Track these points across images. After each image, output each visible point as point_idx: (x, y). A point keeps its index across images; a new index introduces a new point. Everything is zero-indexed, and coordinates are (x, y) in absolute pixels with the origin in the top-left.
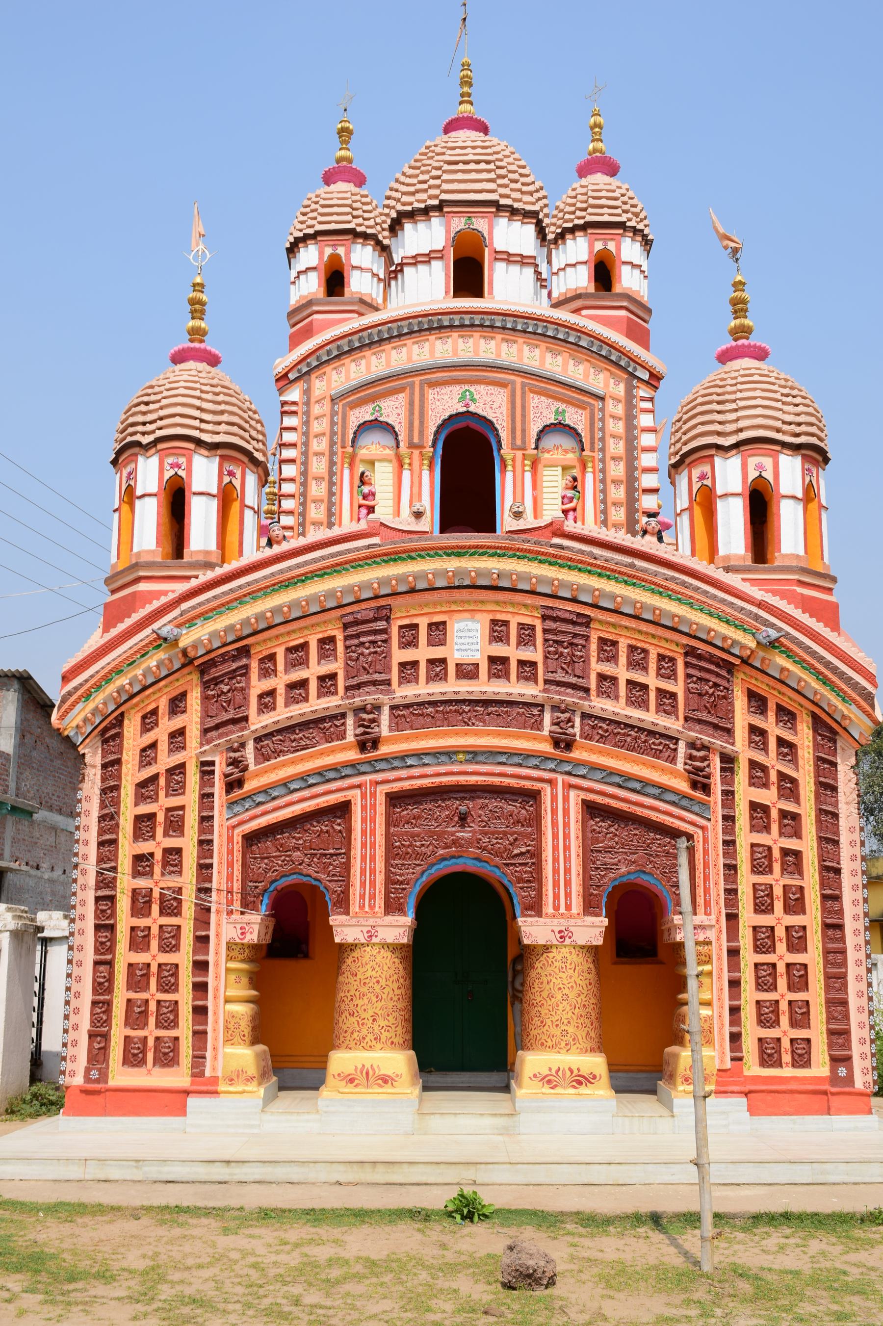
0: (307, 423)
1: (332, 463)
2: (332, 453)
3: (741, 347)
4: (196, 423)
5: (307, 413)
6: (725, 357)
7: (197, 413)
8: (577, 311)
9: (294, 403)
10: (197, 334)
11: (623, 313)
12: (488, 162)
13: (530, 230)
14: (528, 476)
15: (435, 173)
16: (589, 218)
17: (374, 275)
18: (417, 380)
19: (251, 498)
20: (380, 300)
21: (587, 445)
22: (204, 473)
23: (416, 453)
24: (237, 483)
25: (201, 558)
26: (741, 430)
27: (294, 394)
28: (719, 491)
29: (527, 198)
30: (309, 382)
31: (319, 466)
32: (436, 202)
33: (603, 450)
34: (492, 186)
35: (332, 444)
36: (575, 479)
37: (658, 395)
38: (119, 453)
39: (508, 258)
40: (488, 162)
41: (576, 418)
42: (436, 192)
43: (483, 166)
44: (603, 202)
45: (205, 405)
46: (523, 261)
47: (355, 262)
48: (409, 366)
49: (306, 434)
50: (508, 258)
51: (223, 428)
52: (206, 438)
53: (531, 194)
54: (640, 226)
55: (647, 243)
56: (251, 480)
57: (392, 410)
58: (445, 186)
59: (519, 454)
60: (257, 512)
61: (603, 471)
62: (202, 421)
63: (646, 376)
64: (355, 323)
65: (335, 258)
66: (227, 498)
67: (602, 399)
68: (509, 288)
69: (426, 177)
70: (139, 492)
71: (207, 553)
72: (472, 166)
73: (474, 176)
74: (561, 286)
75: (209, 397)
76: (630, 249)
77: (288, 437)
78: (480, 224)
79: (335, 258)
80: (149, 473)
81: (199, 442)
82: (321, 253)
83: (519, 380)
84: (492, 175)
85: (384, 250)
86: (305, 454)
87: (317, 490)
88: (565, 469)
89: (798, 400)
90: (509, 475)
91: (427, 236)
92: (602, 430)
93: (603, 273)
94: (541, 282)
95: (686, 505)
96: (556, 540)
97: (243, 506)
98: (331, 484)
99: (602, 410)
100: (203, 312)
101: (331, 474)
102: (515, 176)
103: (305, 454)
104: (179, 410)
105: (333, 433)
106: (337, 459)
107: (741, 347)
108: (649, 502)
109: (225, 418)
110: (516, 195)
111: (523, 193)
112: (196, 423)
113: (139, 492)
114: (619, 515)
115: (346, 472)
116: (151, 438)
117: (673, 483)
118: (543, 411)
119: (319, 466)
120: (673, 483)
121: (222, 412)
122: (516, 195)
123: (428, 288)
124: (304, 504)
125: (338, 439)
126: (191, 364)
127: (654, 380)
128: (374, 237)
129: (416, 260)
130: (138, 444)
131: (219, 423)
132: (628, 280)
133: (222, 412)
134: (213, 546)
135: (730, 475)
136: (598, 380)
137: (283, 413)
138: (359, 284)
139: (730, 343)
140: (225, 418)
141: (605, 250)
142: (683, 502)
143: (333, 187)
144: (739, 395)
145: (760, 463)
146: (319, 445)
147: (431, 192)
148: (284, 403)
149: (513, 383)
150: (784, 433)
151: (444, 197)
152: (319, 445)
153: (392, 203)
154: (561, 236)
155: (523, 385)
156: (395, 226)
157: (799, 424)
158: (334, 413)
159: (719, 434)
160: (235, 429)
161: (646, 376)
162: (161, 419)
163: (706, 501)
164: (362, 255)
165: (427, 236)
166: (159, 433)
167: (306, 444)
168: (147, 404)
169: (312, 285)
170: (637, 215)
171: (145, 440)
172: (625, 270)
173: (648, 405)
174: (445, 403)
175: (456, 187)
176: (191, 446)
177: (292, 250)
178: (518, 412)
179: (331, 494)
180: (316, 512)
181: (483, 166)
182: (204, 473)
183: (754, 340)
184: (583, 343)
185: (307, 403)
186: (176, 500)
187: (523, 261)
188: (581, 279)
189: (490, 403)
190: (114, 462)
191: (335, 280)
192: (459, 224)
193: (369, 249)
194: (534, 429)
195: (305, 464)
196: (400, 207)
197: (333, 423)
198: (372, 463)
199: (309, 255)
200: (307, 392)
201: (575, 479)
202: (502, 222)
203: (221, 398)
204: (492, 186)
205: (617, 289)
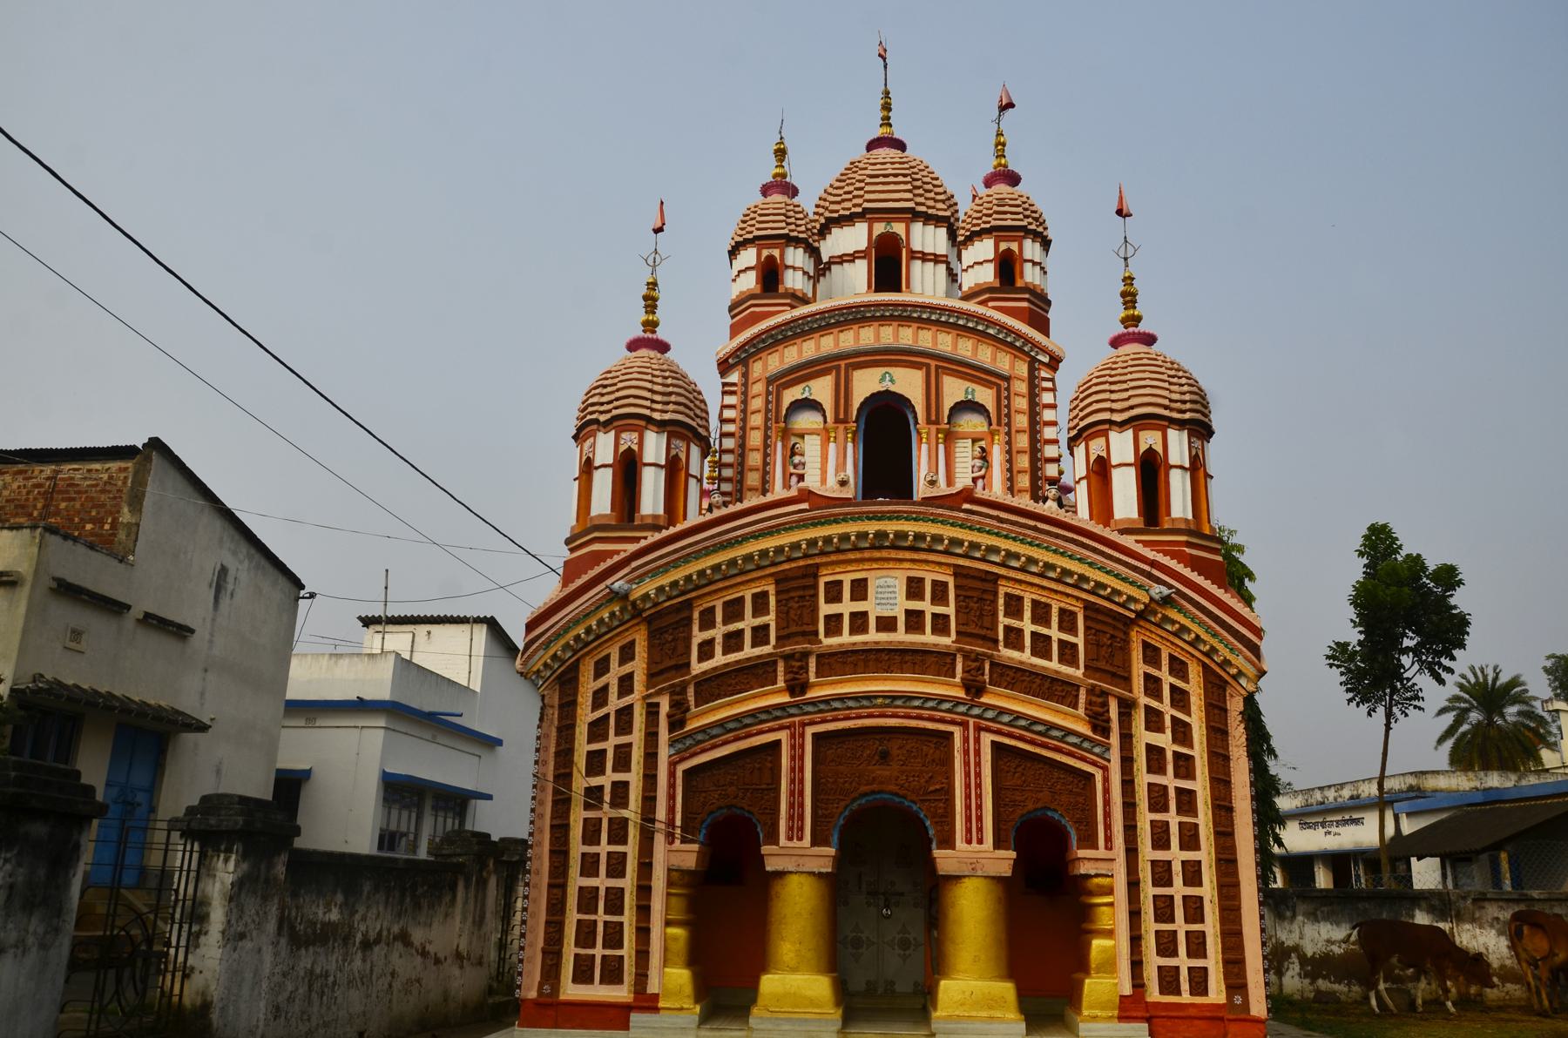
0: (745, 402)
1: (766, 437)
2: (767, 428)
3: (1133, 334)
4: (648, 403)
5: (745, 393)
6: (1116, 342)
7: (648, 395)
8: (980, 303)
9: (734, 384)
10: (651, 325)
11: (1025, 304)
12: (905, 175)
13: (942, 232)
14: (941, 447)
15: (858, 185)
16: (994, 223)
17: (805, 273)
18: (843, 363)
19: (694, 470)
20: (810, 295)
21: (994, 420)
22: (654, 447)
23: (841, 427)
24: (683, 456)
25: (649, 521)
26: (1132, 407)
27: (734, 377)
28: (1114, 462)
29: (940, 205)
30: (747, 366)
31: (755, 438)
32: (859, 210)
33: (1009, 425)
34: (909, 195)
35: (767, 419)
36: (983, 449)
37: (1058, 376)
38: (580, 429)
39: (924, 257)
40: (905, 175)
41: (985, 396)
42: (859, 201)
43: (901, 179)
44: (1006, 209)
45: (657, 388)
46: (937, 259)
47: (789, 262)
48: (836, 351)
49: (744, 411)
50: (924, 257)
51: (671, 407)
52: (657, 416)
53: (943, 201)
54: (1040, 229)
55: (1046, 244)
56: (695, 451)
57: (821, 388)
58: (867, 196)
59: (933, 428)
60: (700, 481)
61: (1009, 443)
62: (653, 401)
63: (1046, 359)
64: (788, 315)
65: (771, 258)
66: (674, 469)
67: (1007, 379)
68: (926, 285)
69: (851, 188)
70: (597, 464)
71: (655, 517)
72: (891, 179)
73: (892, 187)
74: (968, 281)
75: (659, 380)
76: (1031, 249)
77: (728, 414)
78: (899, 228)
79: (771, 258)
80: (605, 447)
81: (649, 420)
82: (759, 255)
83: (933, 363)
84: (909, 187)
85: (814, 252)
86: (743, 428)
87: (755, 459)
88: (974, 441)
89: (1183, 381)
90: (924, 447)
91: (853, 238)
92: (1008, 406)
93: (1007, 266)
94: (952, 276)
95: (1084, 473)
96: (966, 506)
97: (688, 475)
98: (766, 455)
99: (1008, 389)
100: (655, 307)
101: (766, 446)
102: (929, 187)
103: (743, 428)
104: (631, 401)
105: (767, 411)
106: (772, 433)
107: (1133, 334)
108: (1051, 470)
109: (673, 398)
110: (931, 203)
111: (936, 201)
112: (648, 403)
113: (597, 464)
114: (1024, 481)
115: (779, 445)
116: (608, 416)
117: (1072, 454)
118: (954, 390)
119: (755, 438)
120: (1072, 454)
121: (670, 394)
122: (931, 203)
123: (854, 283)
124: (741, 473)
125: (772, 415)
126: (643, 352)
127: (1055, 362)
128: (804, 241)
129: (842, 260)
130: (596, 421)
131: (667, 403)
132: (1030, 275)
133: (670, 394)
134: (661, 511)
135: (1122, 447)
136: (1003, 362)
137: (724, 393)
138: (794, 281)
139: (1120, 329)
140: (673, 398)
141: (1009, 250)
142: (1081, 471)
143: (769, 199)
144: (1129, 377)
145: (1151, 439)
146: (756, 420)
147: (856, 201)
148: (724, 385)
149: (928, 366)
150: (1172, 410)
151: (866, 205)
152: (756, 420)
153: (821, 210)
154: (970, 239)
155: (937, 367)
156: (824, 231)
157: (1184, 402)
158: (768, 393)
159: (1112, 411)
160: (681, 408)
161: (1046, 359)
162: (617, 399)
163: (1101, 470)
164: (795, 256)
165: (853, 238)
166: (615, 412)
167: (744, 420)
168: (605, 386)
169: (750, 282)
170: (1036, 219)
171: (602, 418)
172: (1028, 266)
173: (1049, 385)
174: (866, 383)
175: (878, 197)
176: (643, 423)
177: (733, 253)
178: (933, 393)
179: (765, 464)
180: (753, 479)
181: (901, 179)
182: (654, 447)
183: (1143, 327)
184: (991, 331)
185: (745, 385)
186: (628, 469)
187: (937, 259)
188: (987, 275)
189: (909, 383)
190: (576, 437)
191: (770, 275)
192: (879, 228)
193: (801, 251)
194: (948, 403)
195: (743, 437)
196: (827, 214)
197: (768, 402)
198: (802, 436)
199: (749, 257)
200: (745, 375)
201: (983, 449)
202: (917, 227)
203: (669, 381)
204: (909, 195)
205: (1019, 284)
